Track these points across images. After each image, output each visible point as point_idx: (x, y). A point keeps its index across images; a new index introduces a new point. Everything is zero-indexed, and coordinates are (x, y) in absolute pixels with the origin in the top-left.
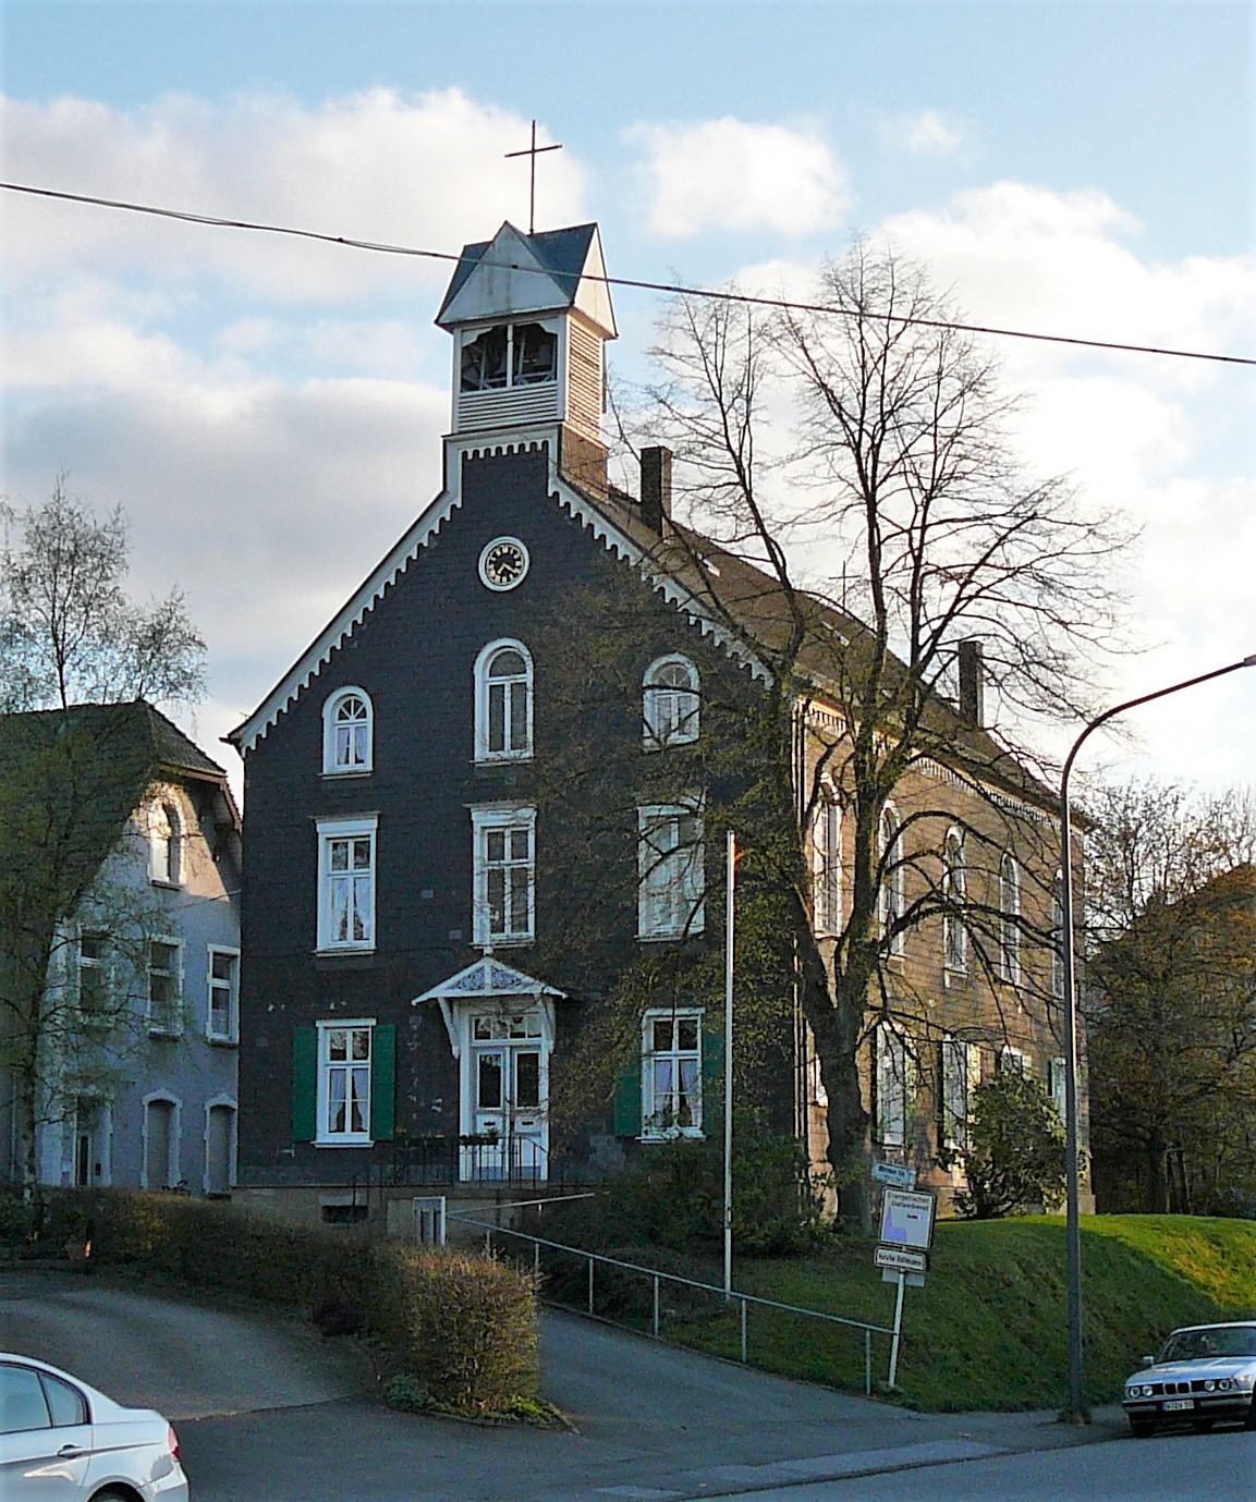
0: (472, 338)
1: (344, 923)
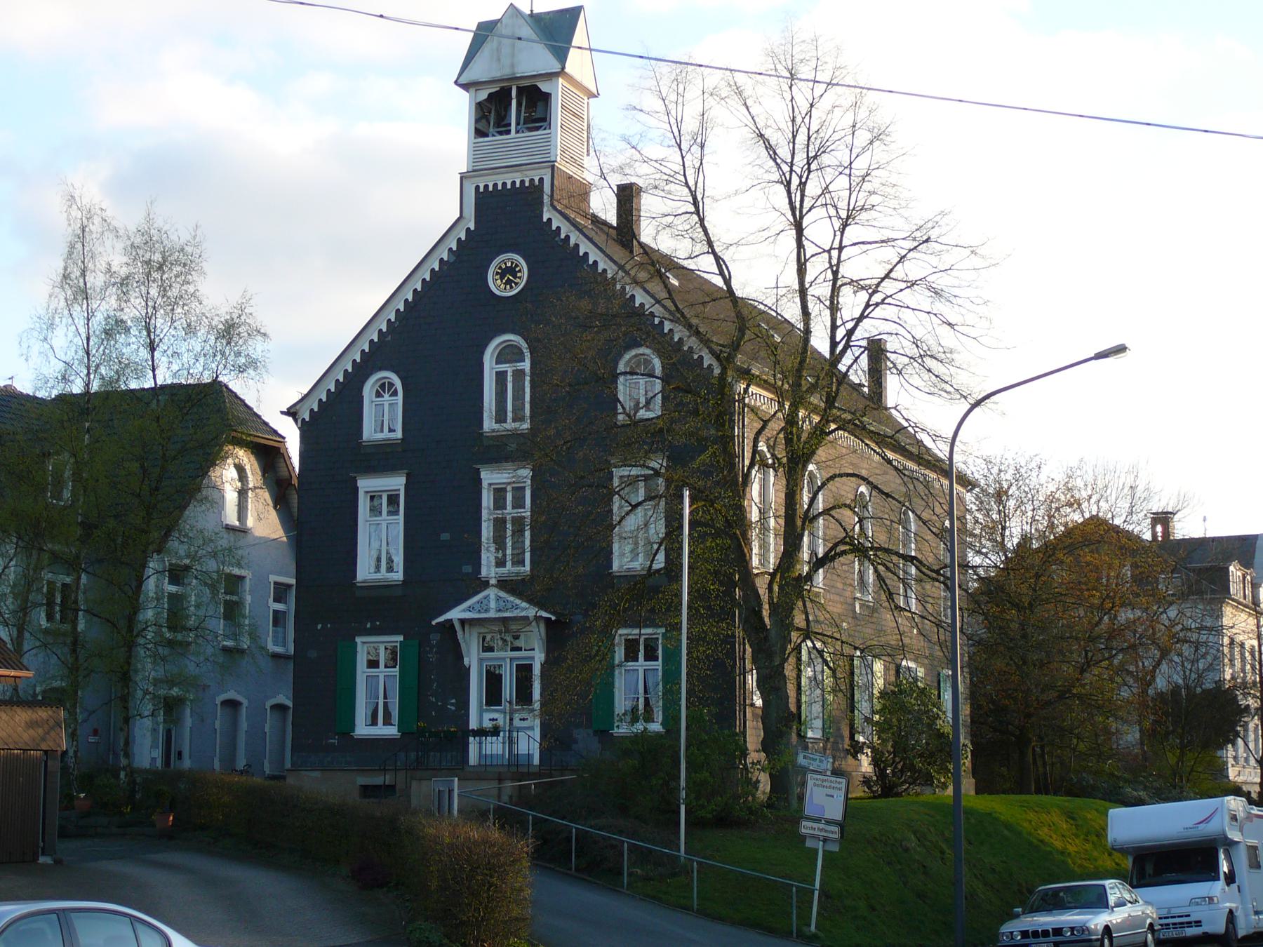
0: (483, 95)
1: (379, 560)
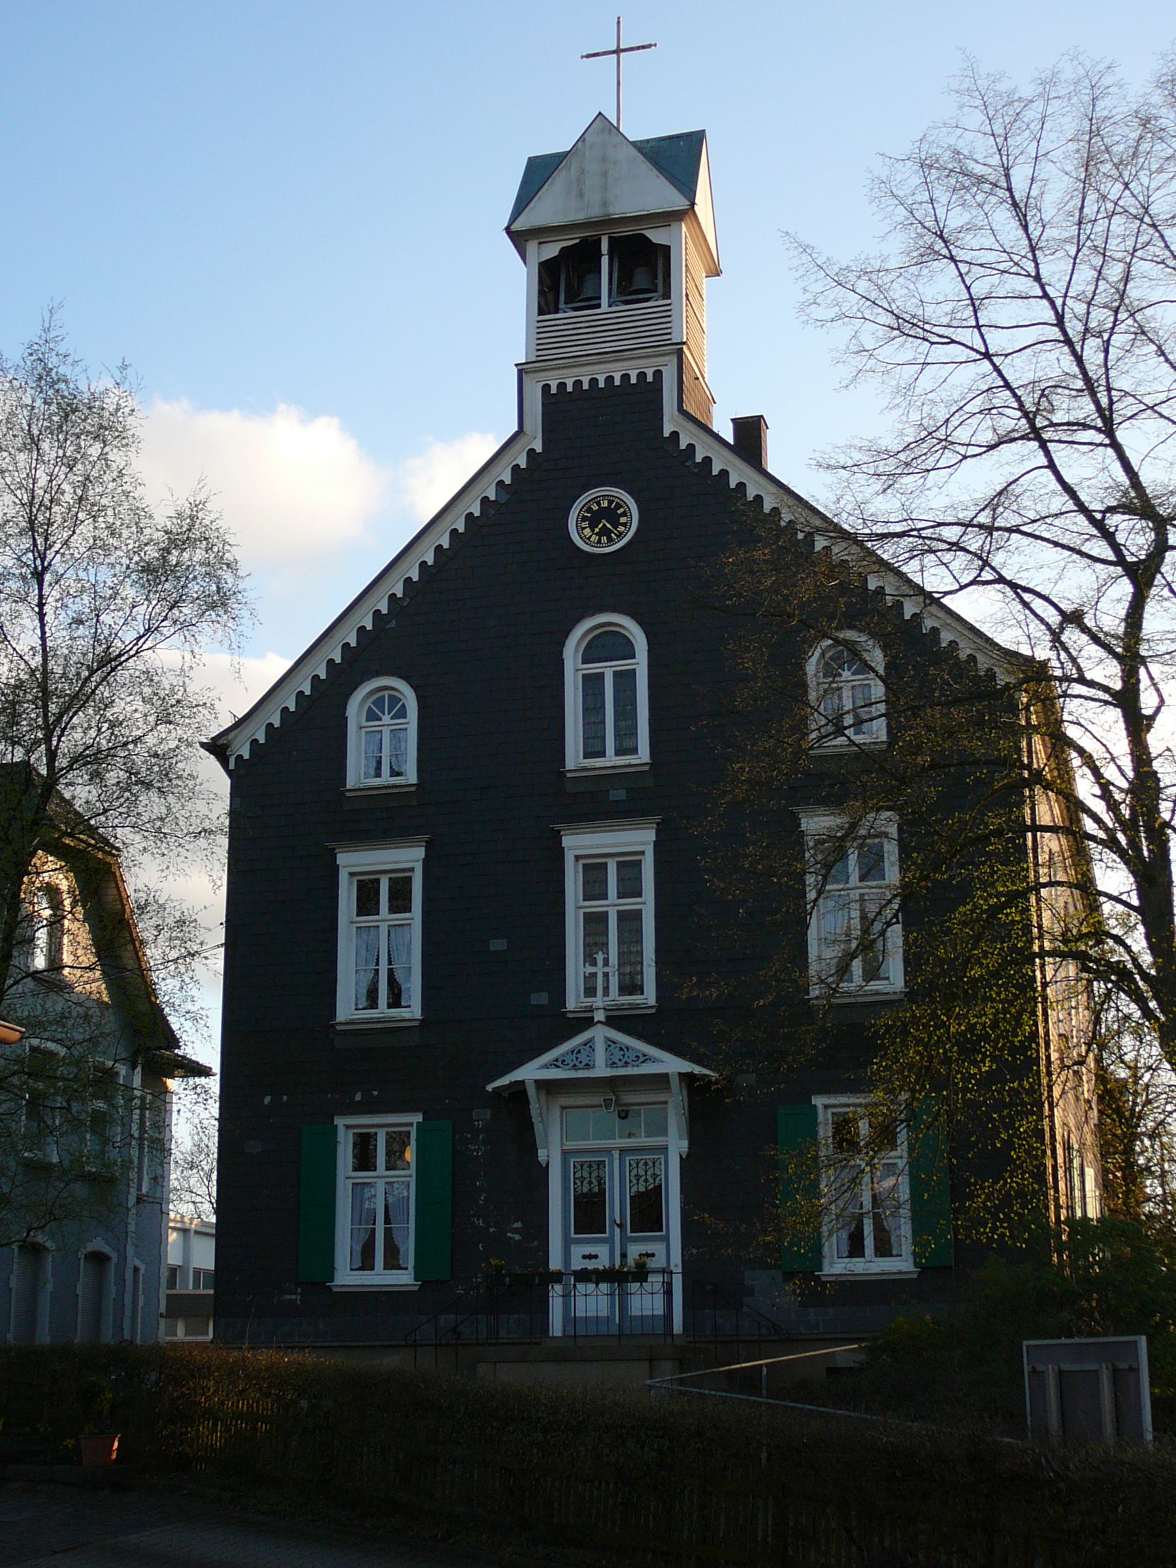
0: (552, 251)
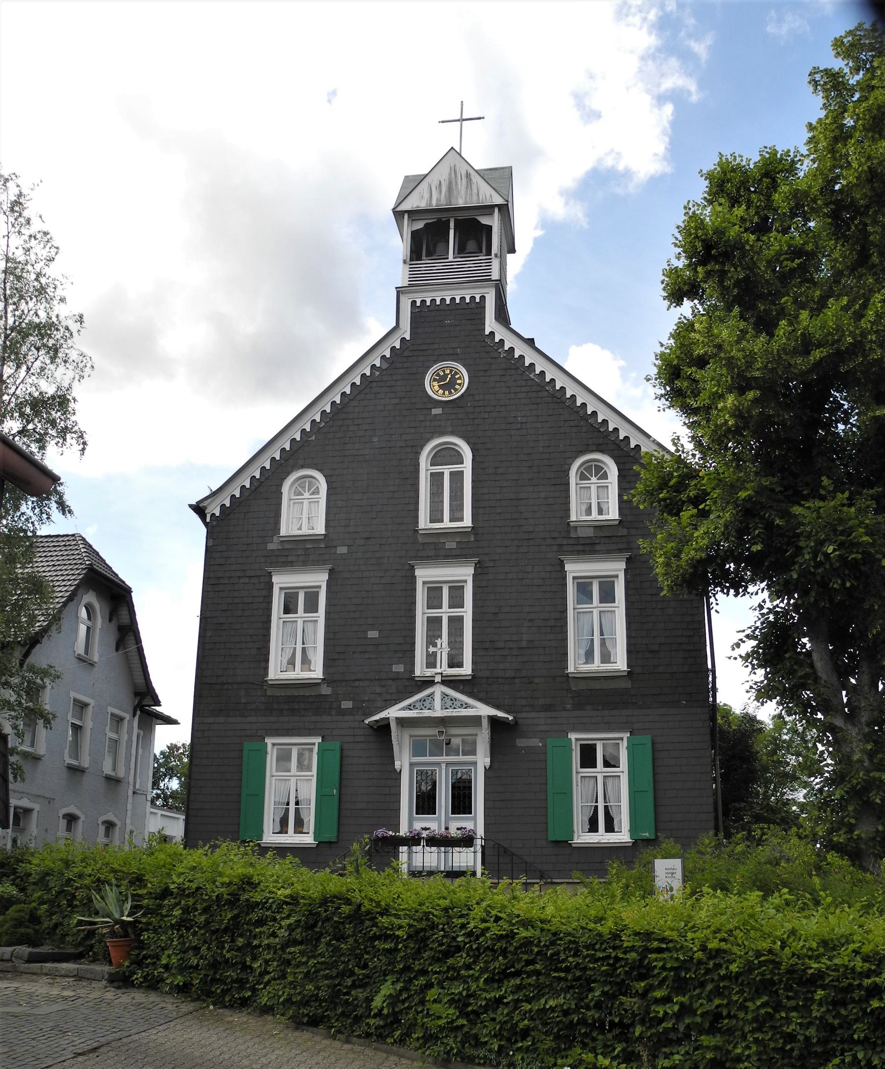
0: (420, 225)
